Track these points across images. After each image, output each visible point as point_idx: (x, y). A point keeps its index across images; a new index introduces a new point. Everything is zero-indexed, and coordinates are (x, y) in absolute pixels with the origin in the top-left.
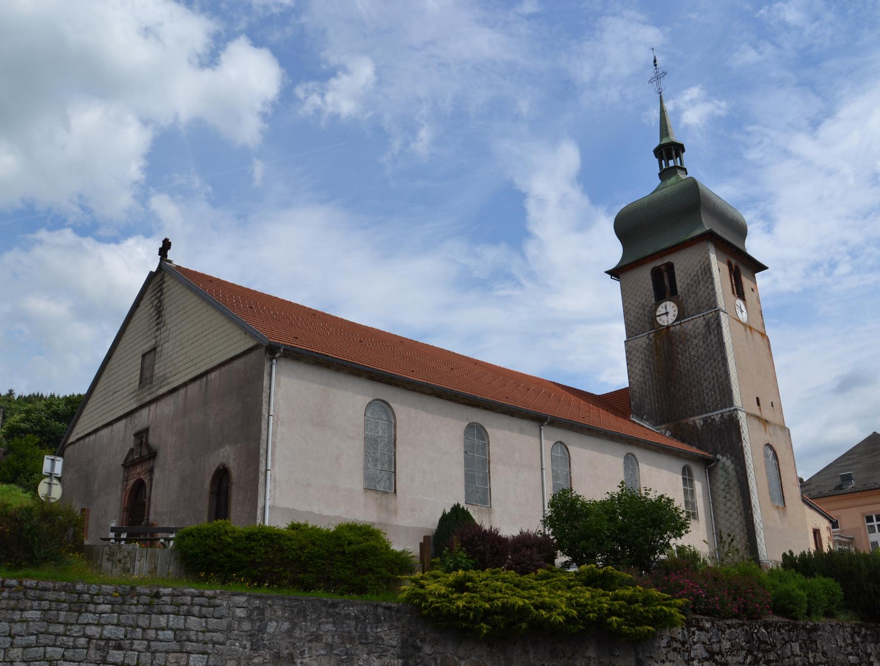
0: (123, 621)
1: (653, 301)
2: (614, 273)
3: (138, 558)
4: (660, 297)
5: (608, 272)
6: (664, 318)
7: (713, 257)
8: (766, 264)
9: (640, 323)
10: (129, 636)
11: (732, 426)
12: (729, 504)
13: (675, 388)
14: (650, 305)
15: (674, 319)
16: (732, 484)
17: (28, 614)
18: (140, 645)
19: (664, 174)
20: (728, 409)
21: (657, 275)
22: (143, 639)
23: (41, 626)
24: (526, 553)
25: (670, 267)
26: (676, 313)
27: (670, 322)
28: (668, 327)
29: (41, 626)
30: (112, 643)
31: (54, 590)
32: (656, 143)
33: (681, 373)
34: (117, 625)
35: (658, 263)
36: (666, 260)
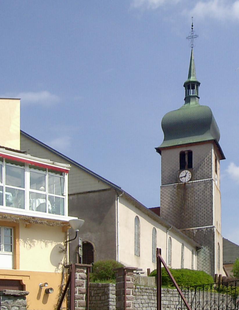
0: (167, 299)
1: (179, 168)
2: (159, 150)
3: (141, 280)
4: (183, 167)
5: (156, 148)
6: (184, 178)
7: (213, 150)
8: (226, 158)
9: (170, 180)
10: (170, 304)
11: (211, 233)
12: (204, 267)
13: (185, 213)
14: (177, 170)
15: (189, 180)
16: (207, 259)
17: (144, 297)
18: (172, 306)
19: (187, 99)
20: (210, 226)
21: (182, 155)
22: (173, 305)
23: (148, 301)
24: (74, 303)
25: (190, 153)
26: (190, 177)
27: (187, 181)
28: (185, 184)
29: (148, 301)
30: (166, 306)
31: (149, 289)
32: (186, 80)
33: (189, 207)
34: (166, 300)
35: (184, 149)
36: (189, 148)
